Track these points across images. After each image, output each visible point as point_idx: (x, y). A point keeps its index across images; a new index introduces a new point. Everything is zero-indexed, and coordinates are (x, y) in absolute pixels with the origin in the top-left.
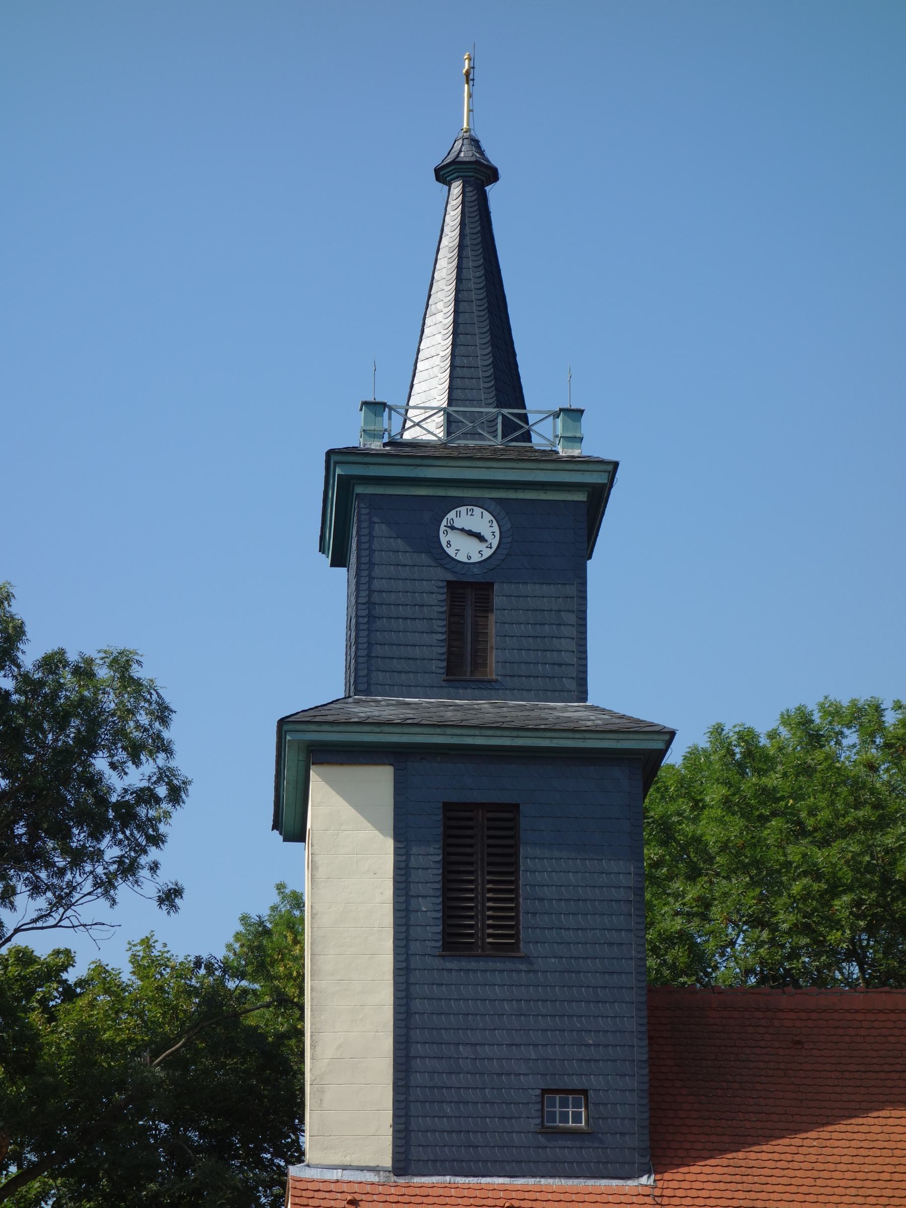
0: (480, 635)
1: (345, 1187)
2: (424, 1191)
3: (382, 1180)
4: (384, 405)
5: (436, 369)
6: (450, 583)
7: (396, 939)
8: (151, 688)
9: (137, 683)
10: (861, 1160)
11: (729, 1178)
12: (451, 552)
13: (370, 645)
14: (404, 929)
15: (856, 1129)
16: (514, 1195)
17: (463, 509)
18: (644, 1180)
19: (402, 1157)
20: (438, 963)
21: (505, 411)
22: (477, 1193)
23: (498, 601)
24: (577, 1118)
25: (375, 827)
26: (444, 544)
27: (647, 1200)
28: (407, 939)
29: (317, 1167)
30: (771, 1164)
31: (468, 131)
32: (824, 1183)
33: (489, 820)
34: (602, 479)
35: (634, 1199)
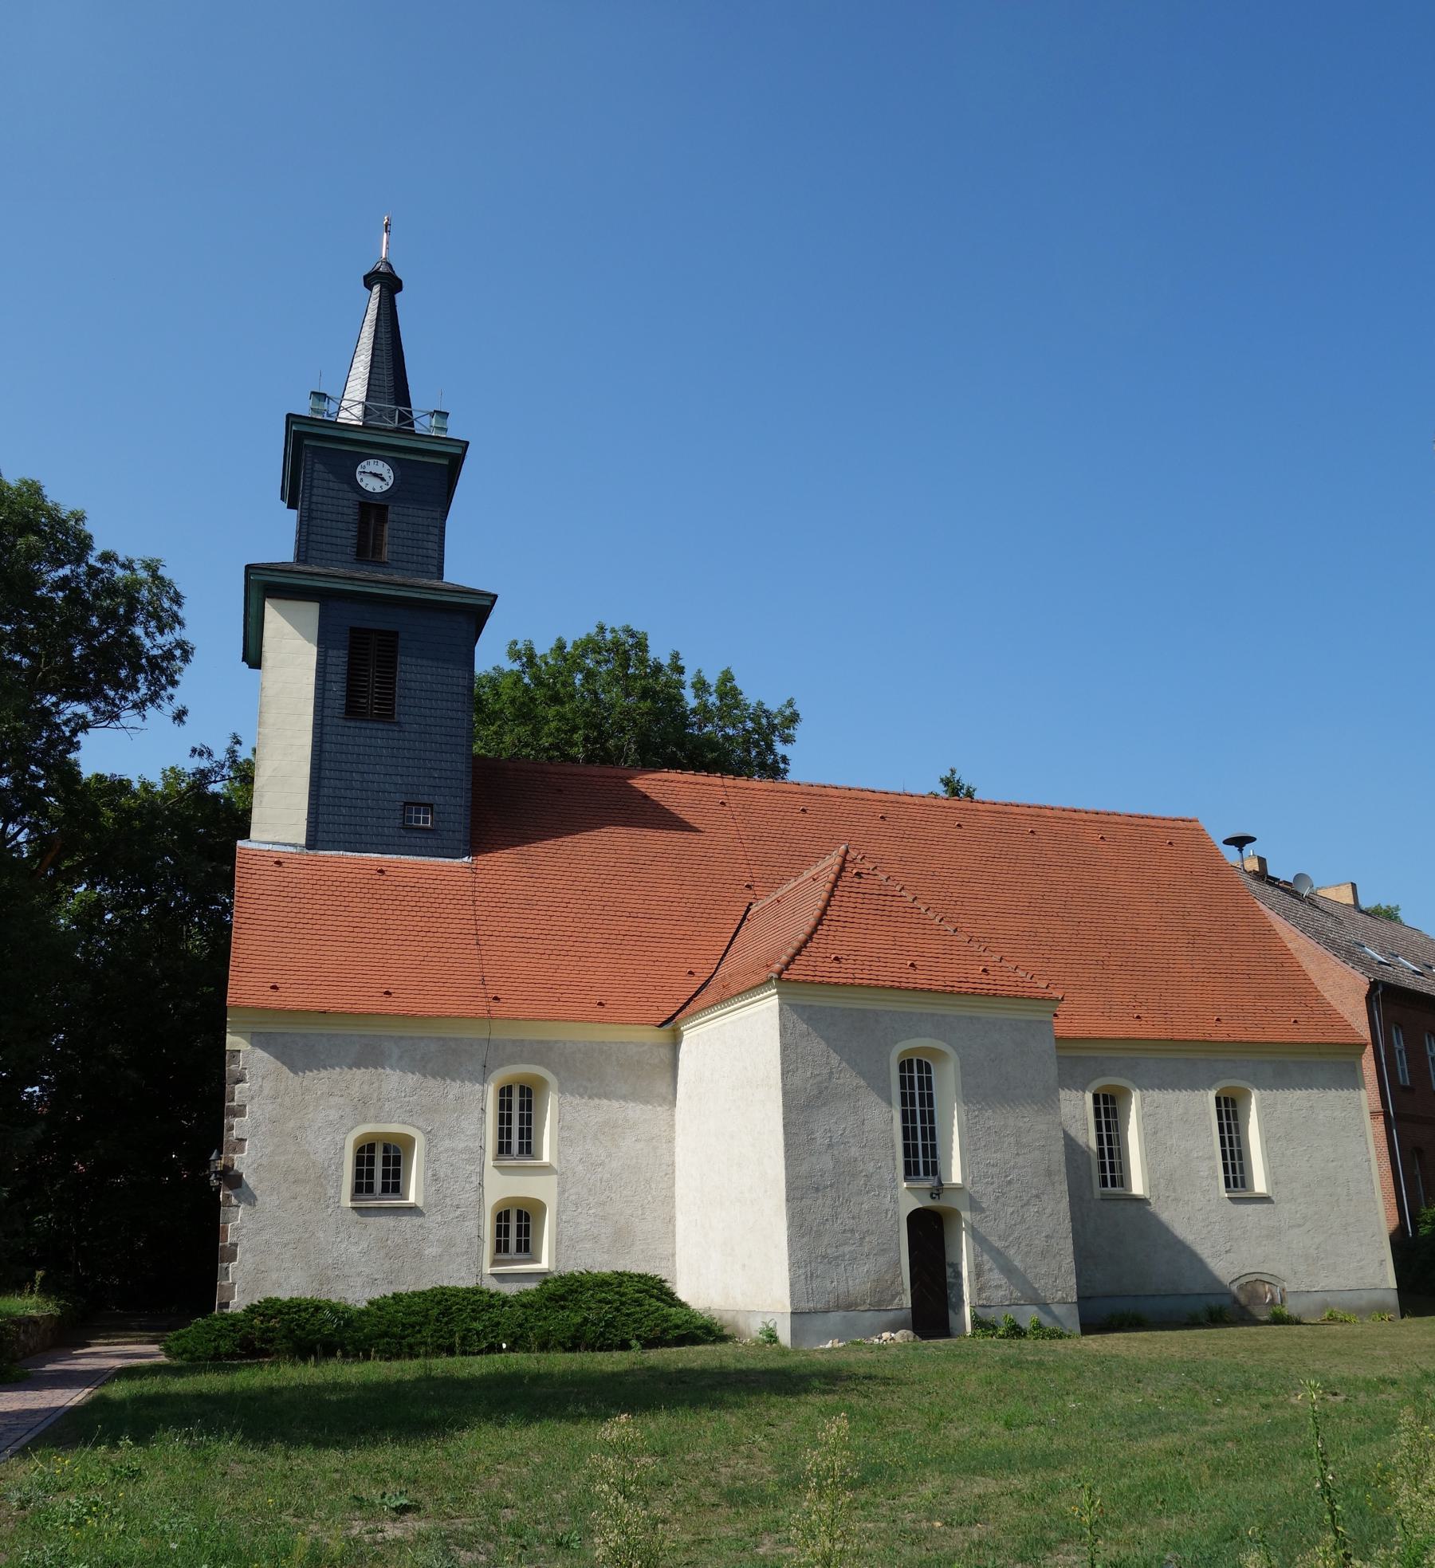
0: (379, 536)
1: (274, 854)
2: (326, 859)
3: (298, 851)
4: (325, 395)
5: (359, 387)
6: (361, 504)
7: (315, 706)
8: (170, 585)
9: (161, 579)
10: (597, 855)
11: (518, 861)
12: (363, 484)
13: (308, 534)
14: (321, 700)
15: (594, 838)
16: (383, 864)
17: (372, 461)
18: (466, 859)
19: (317, 767)
20: (342, 722)
21: (401, 408)
22: (360, 862)
23: (390, 516)
24: (425, 821)
25: (304, 637)
26: (359, 480)
27: (467, 870)
28: (323, 707)
29: (255, 842)
30: (544, 854)
31: (385, 258)
32: (575, 866)
33: (379, 640)
34: (458, 451)
35: (459, 870)
